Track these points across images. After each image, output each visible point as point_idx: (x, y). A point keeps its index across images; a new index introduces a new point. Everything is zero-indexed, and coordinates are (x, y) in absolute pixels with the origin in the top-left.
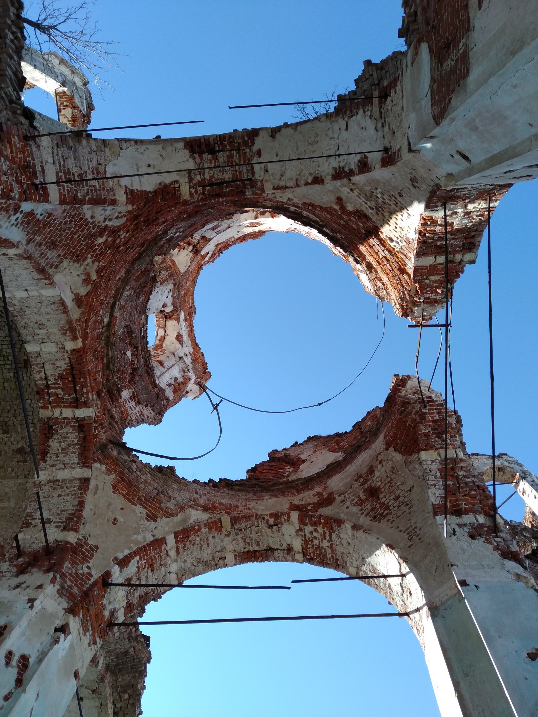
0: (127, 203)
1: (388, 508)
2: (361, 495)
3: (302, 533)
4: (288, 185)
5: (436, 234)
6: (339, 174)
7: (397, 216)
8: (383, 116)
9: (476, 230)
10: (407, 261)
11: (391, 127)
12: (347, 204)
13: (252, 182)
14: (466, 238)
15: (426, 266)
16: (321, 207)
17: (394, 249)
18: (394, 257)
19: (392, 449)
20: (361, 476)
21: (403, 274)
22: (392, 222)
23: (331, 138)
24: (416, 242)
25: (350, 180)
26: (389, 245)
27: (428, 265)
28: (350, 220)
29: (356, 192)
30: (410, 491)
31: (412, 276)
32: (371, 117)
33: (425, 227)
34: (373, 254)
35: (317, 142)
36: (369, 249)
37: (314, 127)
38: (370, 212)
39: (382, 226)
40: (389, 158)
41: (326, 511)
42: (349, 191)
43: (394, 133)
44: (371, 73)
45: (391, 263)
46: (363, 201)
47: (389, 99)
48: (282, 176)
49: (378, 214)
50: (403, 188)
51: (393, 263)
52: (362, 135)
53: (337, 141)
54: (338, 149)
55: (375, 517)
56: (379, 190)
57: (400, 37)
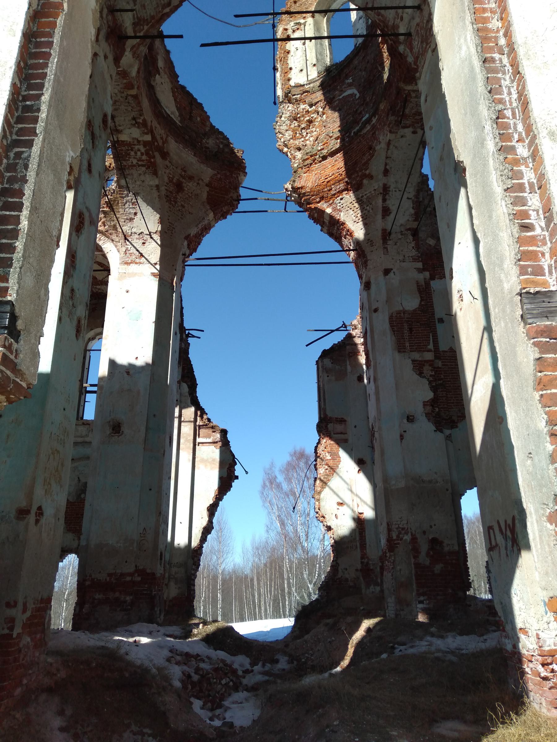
0: (410, 543)
1: (176, 202)
2: (175, 179)
3: (136, 142)
4: (389, 151)
6: (386, 189)
13: (398, 123)
16: (369, 160)
19: (207, 189)
20: (185, 171)
26: (339, 196)
28: (358, 176)
30: (190, 213)
41: (158, 159)
48: (396, 147)
55: (167, 196)
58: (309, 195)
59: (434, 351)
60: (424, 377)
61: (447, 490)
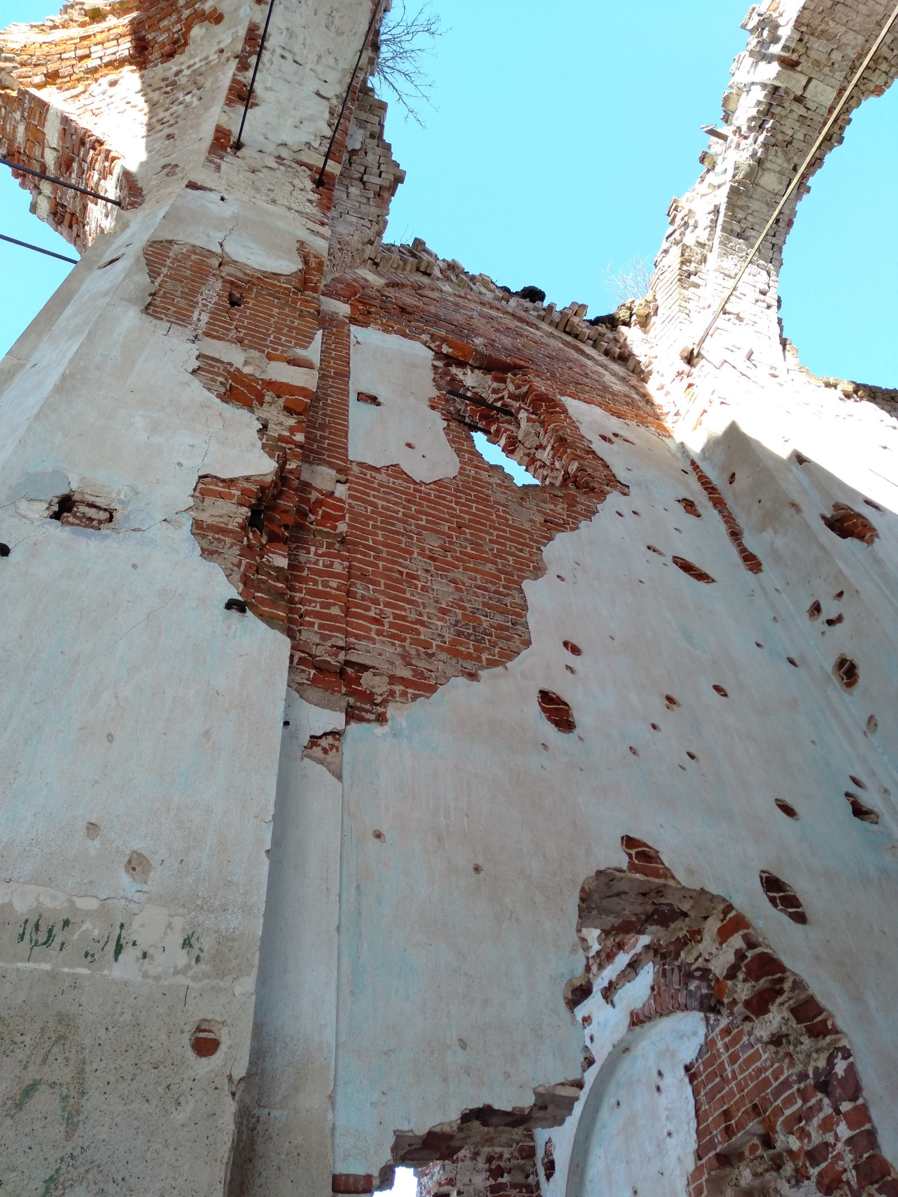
5: (89, 169)
7: (145, 114)
8: (295, 165)
9: (78, 236)
10: (68, 94)
11: (266, 170)
12: (204, 30)
14: (73, 215)
15: (44, 126)
17: (96, 80)
18: (82, 74)
21: (45, 75)
22: (140, 101)
23: (320, 57)
24: (89, 127)
25: (236, 57)
27: (46, 130)
28: (179, 20)
29: (214, 57)
31: (33, 91)
32: (308, 144)
33: (103, 155)
34: (104, 35)
35: (327, 27)
36: (115, 31)
37: (354, 35)
38: (173, 66)
39: (142, 77)
40: (225, 143)
42: (222, 46)
43: (253, 172)
44: (383, 175)
45: (74, 62)
46: (195, 63)
47: (310, 185)
49: (163, 80)
50: (175, 146)
51: (73, 66)
52: (292, 112)
53: (308, 67)
54: (295, 62)
56: (196, 102)
57: (416, 239)
58: (11, 60)
59: (321, 369)
60: (186, 35)
61: (205, 1046)
